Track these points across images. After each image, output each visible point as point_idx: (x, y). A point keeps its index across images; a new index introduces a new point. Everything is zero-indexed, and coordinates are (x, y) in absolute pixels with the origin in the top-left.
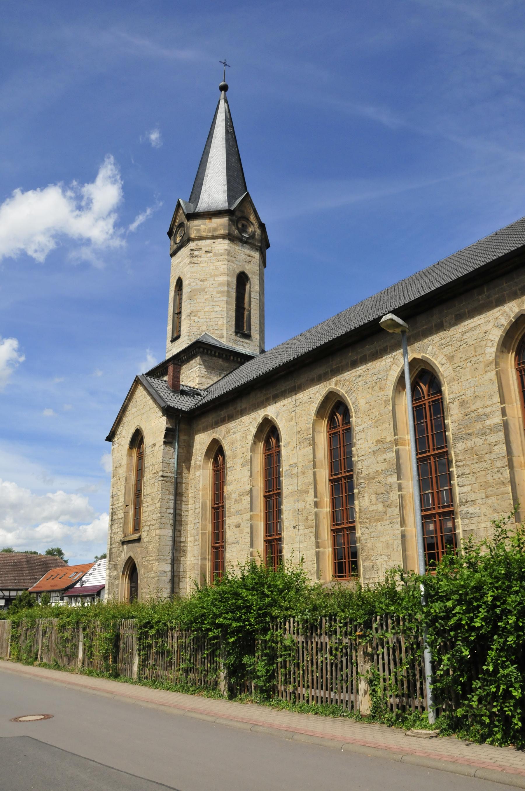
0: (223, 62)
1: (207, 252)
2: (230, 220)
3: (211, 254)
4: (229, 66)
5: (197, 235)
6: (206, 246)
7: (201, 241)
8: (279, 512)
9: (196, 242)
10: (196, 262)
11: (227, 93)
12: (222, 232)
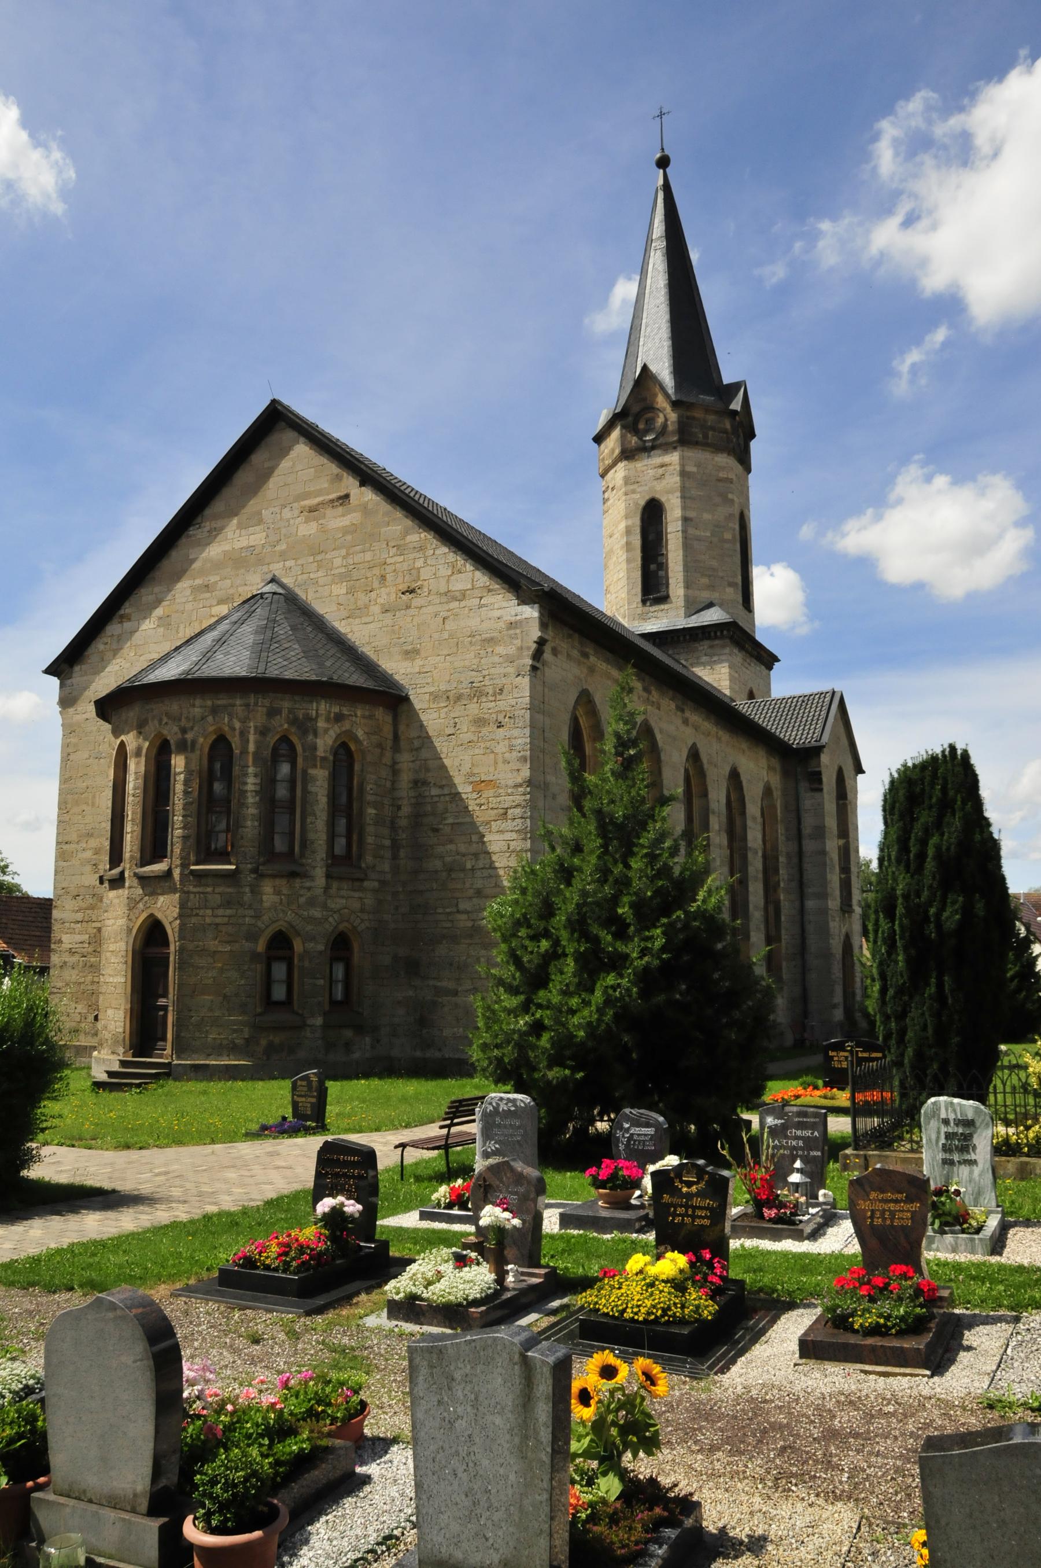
0: (664, 111)
11: (668, 170)
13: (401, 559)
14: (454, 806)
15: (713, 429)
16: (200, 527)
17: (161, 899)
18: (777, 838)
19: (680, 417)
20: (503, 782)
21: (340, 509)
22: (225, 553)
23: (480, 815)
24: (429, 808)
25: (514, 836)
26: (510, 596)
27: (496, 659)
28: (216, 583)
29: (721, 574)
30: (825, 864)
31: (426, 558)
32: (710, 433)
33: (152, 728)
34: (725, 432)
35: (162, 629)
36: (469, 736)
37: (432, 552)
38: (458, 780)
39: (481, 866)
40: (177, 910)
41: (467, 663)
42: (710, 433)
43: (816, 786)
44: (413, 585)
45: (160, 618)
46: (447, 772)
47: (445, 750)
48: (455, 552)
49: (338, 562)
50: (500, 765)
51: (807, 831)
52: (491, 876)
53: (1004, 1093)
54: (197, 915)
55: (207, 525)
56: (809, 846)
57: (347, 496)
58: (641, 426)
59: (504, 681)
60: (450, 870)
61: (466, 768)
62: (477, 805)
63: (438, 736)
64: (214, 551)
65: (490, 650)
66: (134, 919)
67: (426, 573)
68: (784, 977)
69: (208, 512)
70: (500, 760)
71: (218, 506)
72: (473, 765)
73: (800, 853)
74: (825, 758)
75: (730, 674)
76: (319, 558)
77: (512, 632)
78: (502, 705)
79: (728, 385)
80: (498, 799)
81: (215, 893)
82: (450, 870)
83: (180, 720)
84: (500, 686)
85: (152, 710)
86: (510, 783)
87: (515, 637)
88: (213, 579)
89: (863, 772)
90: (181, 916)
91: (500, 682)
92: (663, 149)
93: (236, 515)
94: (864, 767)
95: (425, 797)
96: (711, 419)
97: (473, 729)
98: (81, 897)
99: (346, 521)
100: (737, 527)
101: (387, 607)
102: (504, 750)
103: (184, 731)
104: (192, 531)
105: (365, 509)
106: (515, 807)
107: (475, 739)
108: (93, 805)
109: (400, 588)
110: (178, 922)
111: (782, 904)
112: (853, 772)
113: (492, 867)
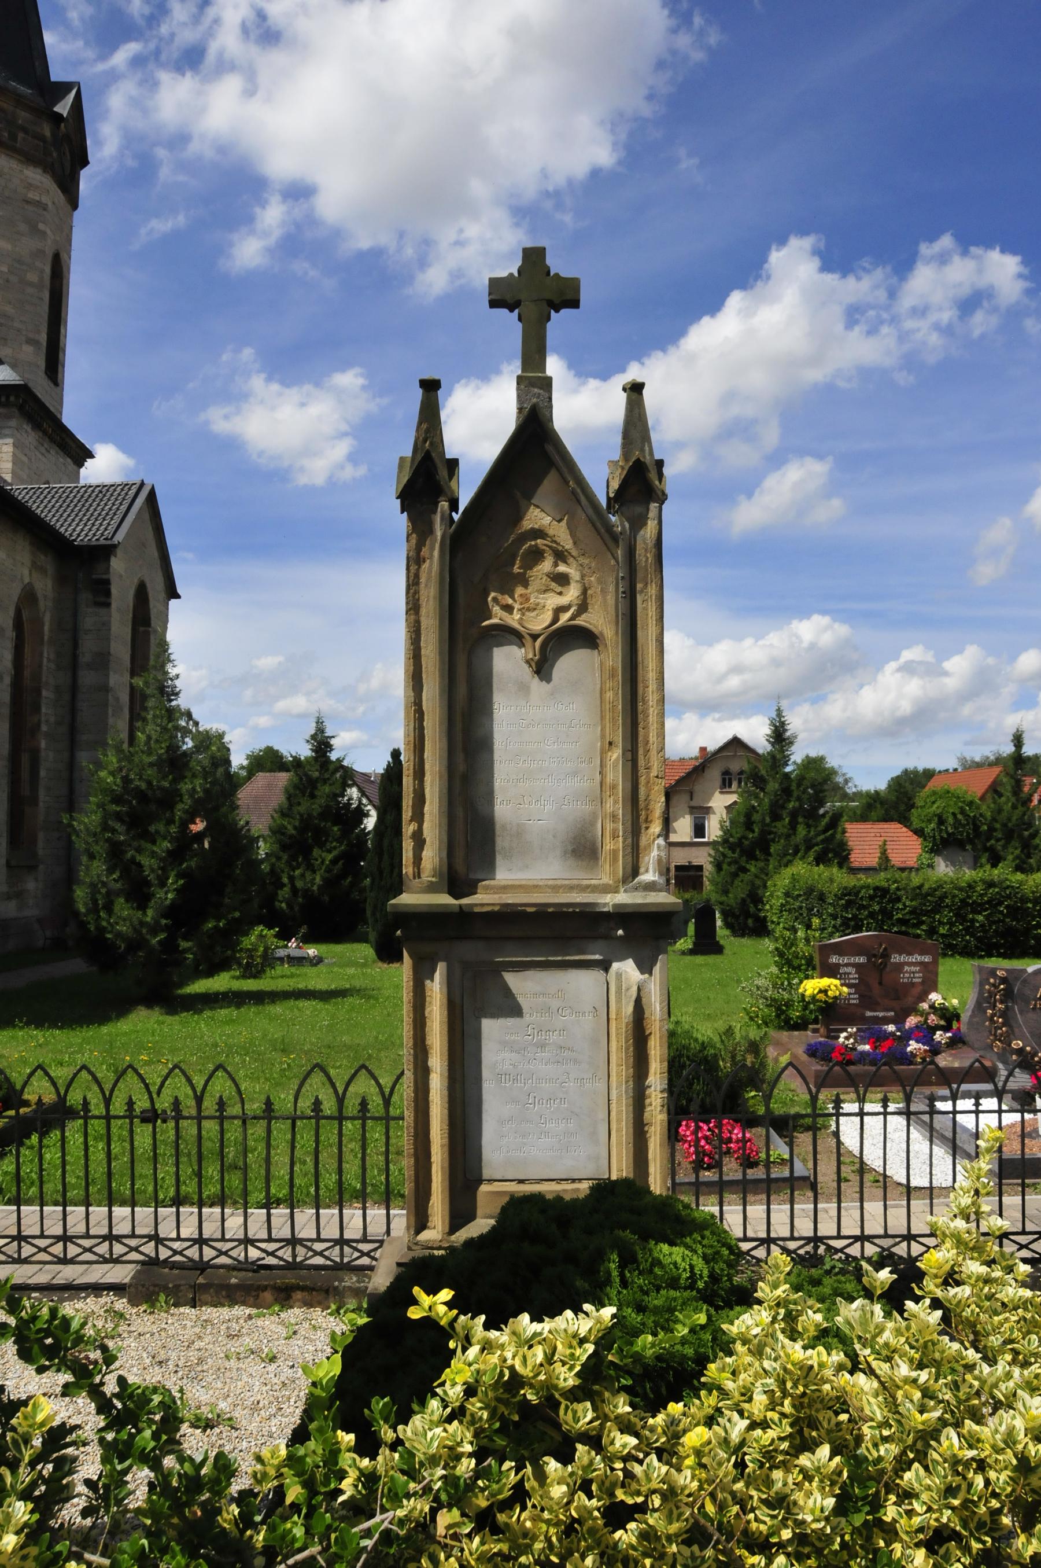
15: (25, 131)
18: (40, 666)
29: (16, 324)
30: (106, 705)
32: (21, 135)
34: (42, 138)
42: (21, 135)
43: (102, 599)
51: (85, 658)
53: (108, 1118)
56: (87, 678)
68: (40, 852)
73: (74, 688)
74: (117, 564)
75: (14, 455)
79: (480, 1024)
89: (177, 596)
94: (179, 591)
96: (23, 116)
100: (48, 270)
111: (43, 754)
112: (162, 595)
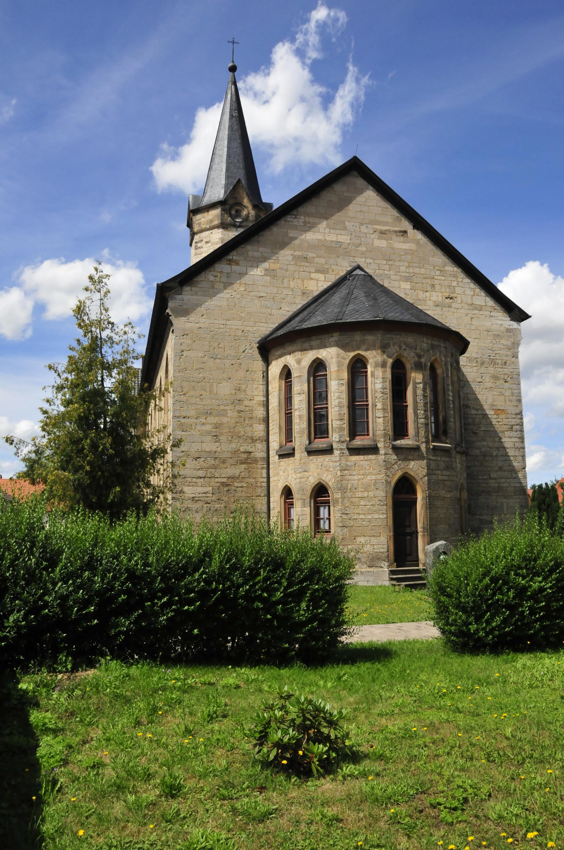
0: (232, 40)
1: (207, 242)
2: (223, 210)
3: (210, 244)
4: (238, 43)
5: (199, 228)
6: (206, 237)
7: (202, 234)
8: (358, 454)
9: (199, 235)
10: (199, 253)
11: (235, 73)
12: (216, 222)
13: (443, 278)
14: (485, 421)
16: (296, 218)
17: (412, 463)
19: (256, 214)
20: (510, 411)
21: (402, 238)
22: (319, 240)
23: (499, 428)
24: (470, 420)
25: (517, 440)
26: (505, 314)
27: (502, 346)
28: (313, 258)
31: (458, 282)
33: (393, 349)
35: (269, 278)
36: (490, 385)
37: (461, 280)
38: (485, 407)
39: (501, 454)
40: (426, 471)
41: (486, 345)
44: (452, 295)
45: (266, 270)
46: (480, 402)
47: (477, 390)
48: (474, 284)
49: (403, 269)
50: (508, 402)
52: (506, 460)
54: (435, 474)
55: (302, 219)
57: (405, 232)
58: (233, 212)
59: (506, 358)
60: (485, 456)
61: (490, 401)
62: (497, 422)
63: (473, 381)
64: (310, 236)
65: (498, 341)
66: (391, 476)
67: (458, 290)
69: (301, 209)
70: (507, 400)
71: (309, 207)
72: (493, 400)
76: (390, 263)
77: (508, 334)
78: (506, 371)
80: (508, 420)
81: (443, 460)
82: (485, 456)
83: (416, 349)
84: (505, 361)
85: (392, 339)
86: (513, 412)
87: (510, 337)
88: (310, 255)
90: (428, 474)
91: (505, 358)
92: (233, 62)
93: (327, 219)
95: (468, 414)
97: (492, 381)
98: (202, 459)
99: (407, 246)
101: (437, 303)
102: (509, 395)
103: (419, 356)
104: (289, 218)
105: (417, 242)
106: (517, 425)
107: (494, 386)
108: (211, 392)
109: (445, 294)
110: (426, 478)
113: (506, 455)
